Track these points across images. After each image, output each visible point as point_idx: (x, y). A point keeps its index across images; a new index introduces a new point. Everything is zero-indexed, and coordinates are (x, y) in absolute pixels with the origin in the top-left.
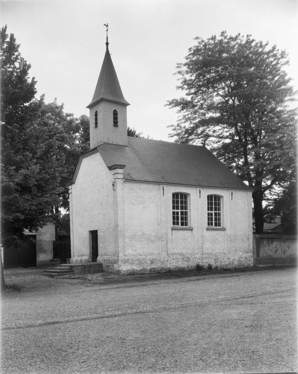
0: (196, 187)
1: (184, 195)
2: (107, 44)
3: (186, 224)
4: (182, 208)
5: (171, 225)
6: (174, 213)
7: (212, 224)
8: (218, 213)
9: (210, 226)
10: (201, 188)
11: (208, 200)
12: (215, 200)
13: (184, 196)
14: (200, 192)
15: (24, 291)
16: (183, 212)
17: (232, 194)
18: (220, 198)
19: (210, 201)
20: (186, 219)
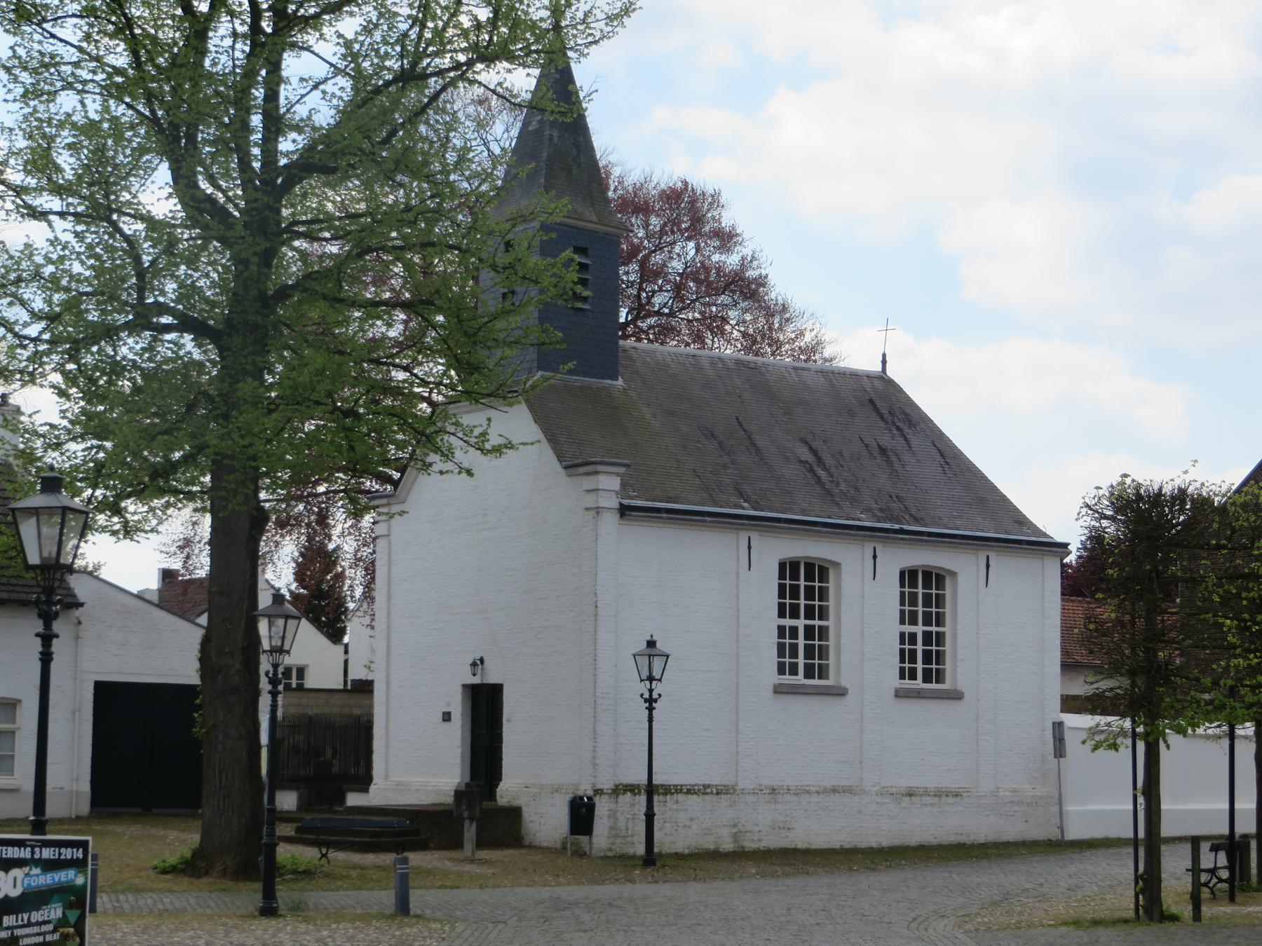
1: (819, 566)
4: (927, 622)
5: (774, 678)
6: (781, 630)
8: (937, 633)
12: (809, 577)
13: (818, 571)
14: (875, 557)
15: (767, 892)
18: (944, 578)
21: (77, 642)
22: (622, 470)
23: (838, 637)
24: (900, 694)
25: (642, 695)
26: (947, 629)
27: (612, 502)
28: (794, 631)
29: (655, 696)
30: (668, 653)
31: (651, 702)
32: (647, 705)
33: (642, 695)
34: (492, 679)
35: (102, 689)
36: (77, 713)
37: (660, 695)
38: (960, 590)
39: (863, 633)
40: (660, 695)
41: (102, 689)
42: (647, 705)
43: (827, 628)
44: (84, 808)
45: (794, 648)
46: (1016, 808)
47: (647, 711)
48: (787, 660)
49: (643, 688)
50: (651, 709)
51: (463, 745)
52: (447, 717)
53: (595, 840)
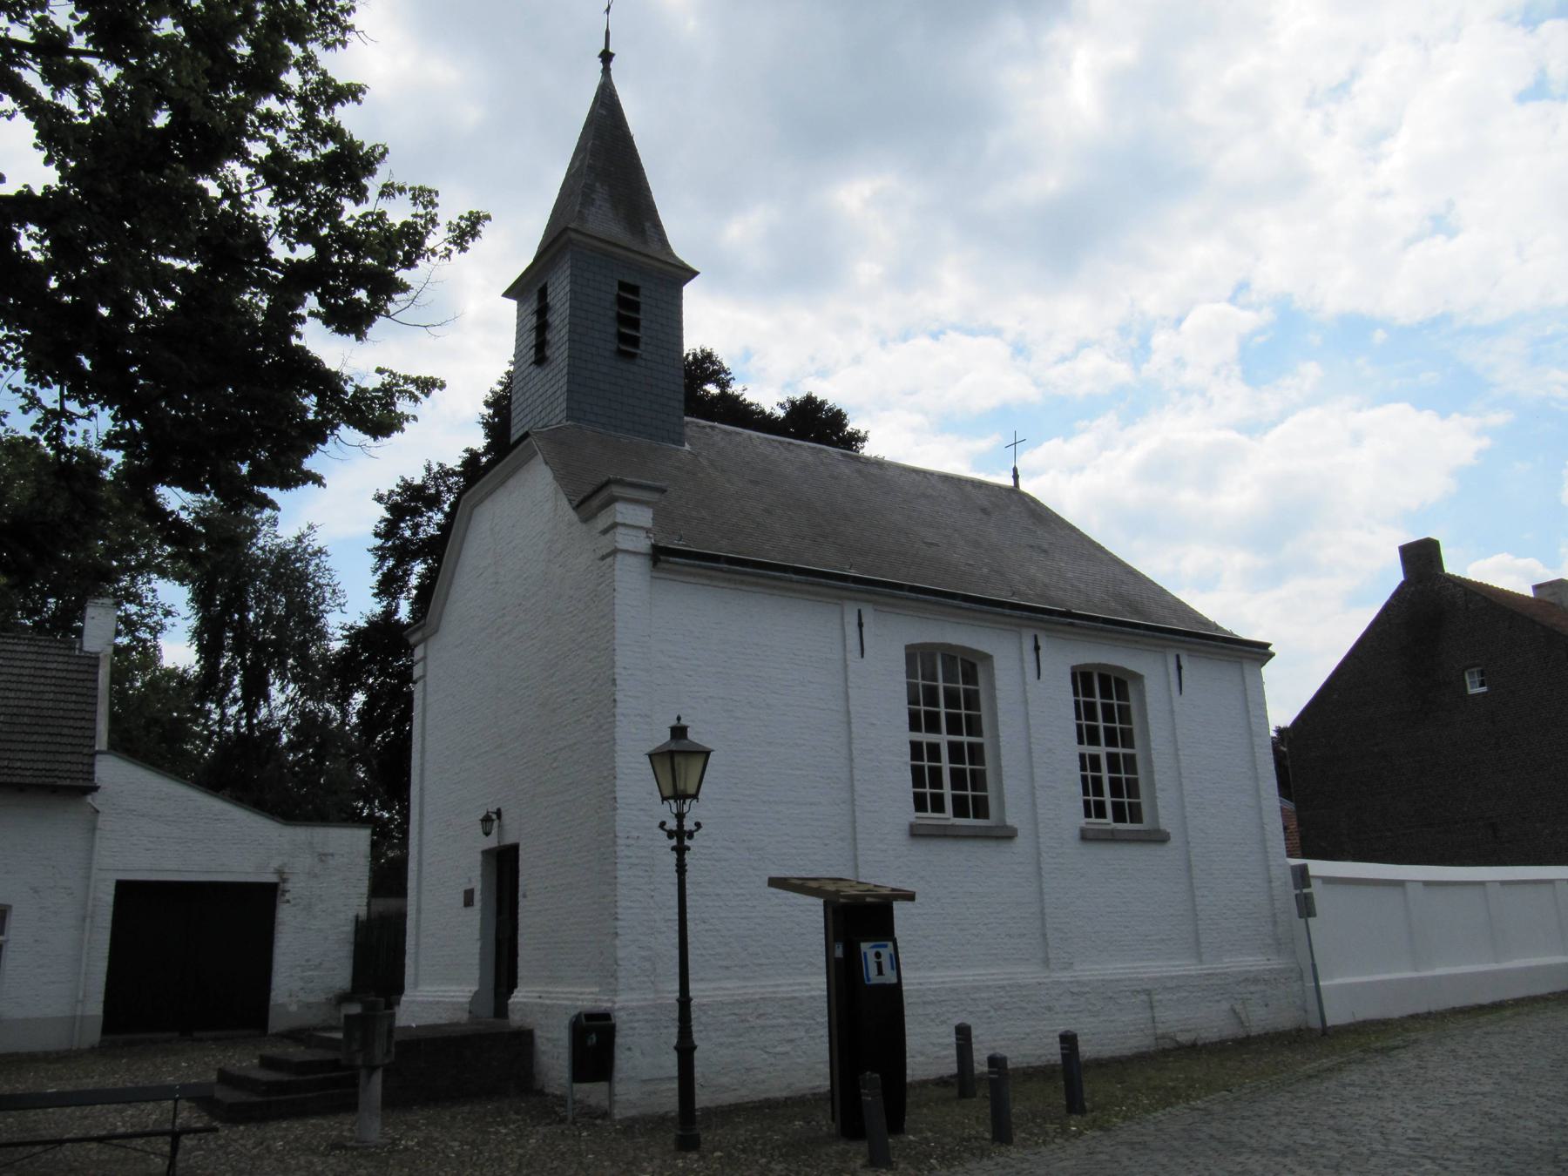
0: (840, 598)
1: (1117, 680)
2: (606, 57)
3: (1136, 817)
5: (909, 814)
6: (916, 748)
7: (938, 805)
9: (929, 814)
10: (1041, 628)
11: (911, 672)
14: (1037, 648)
16: (961, 744)
17: (860, 625)
19: (920, 682)
20: (979, 780)
21: (94, 834)
22: (655, 497)
23: (997, 757)
24: (1086, 837)
25: (662, 825)
26: (1137, 751)
27: (643, 544)
28: (934, 750)
29: (688, 825)
30: (709, 746)
31: (680, 837)
32: (674, 842)
33: (662, 825)
34: (509, 840)
35: (130, 894)
36: (88, 920)
37: (698, 825)
38: (1150, 698)
39: (1030, 752)
40: (698, 825)
41: (130, 894)
42: (674, 842)
43: (981, 746)
44: (94, 1035)
45: (936, 775)
46: (1252, 988)
47: (675, 855)
48: (928, 790)
49: (667, 812)
50: (681, 850)
51: (483, 937)
52: (468, 899)
53: (619, 1088)
